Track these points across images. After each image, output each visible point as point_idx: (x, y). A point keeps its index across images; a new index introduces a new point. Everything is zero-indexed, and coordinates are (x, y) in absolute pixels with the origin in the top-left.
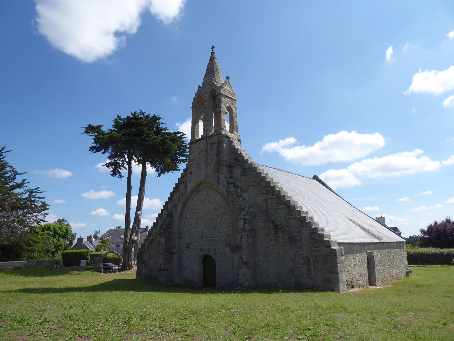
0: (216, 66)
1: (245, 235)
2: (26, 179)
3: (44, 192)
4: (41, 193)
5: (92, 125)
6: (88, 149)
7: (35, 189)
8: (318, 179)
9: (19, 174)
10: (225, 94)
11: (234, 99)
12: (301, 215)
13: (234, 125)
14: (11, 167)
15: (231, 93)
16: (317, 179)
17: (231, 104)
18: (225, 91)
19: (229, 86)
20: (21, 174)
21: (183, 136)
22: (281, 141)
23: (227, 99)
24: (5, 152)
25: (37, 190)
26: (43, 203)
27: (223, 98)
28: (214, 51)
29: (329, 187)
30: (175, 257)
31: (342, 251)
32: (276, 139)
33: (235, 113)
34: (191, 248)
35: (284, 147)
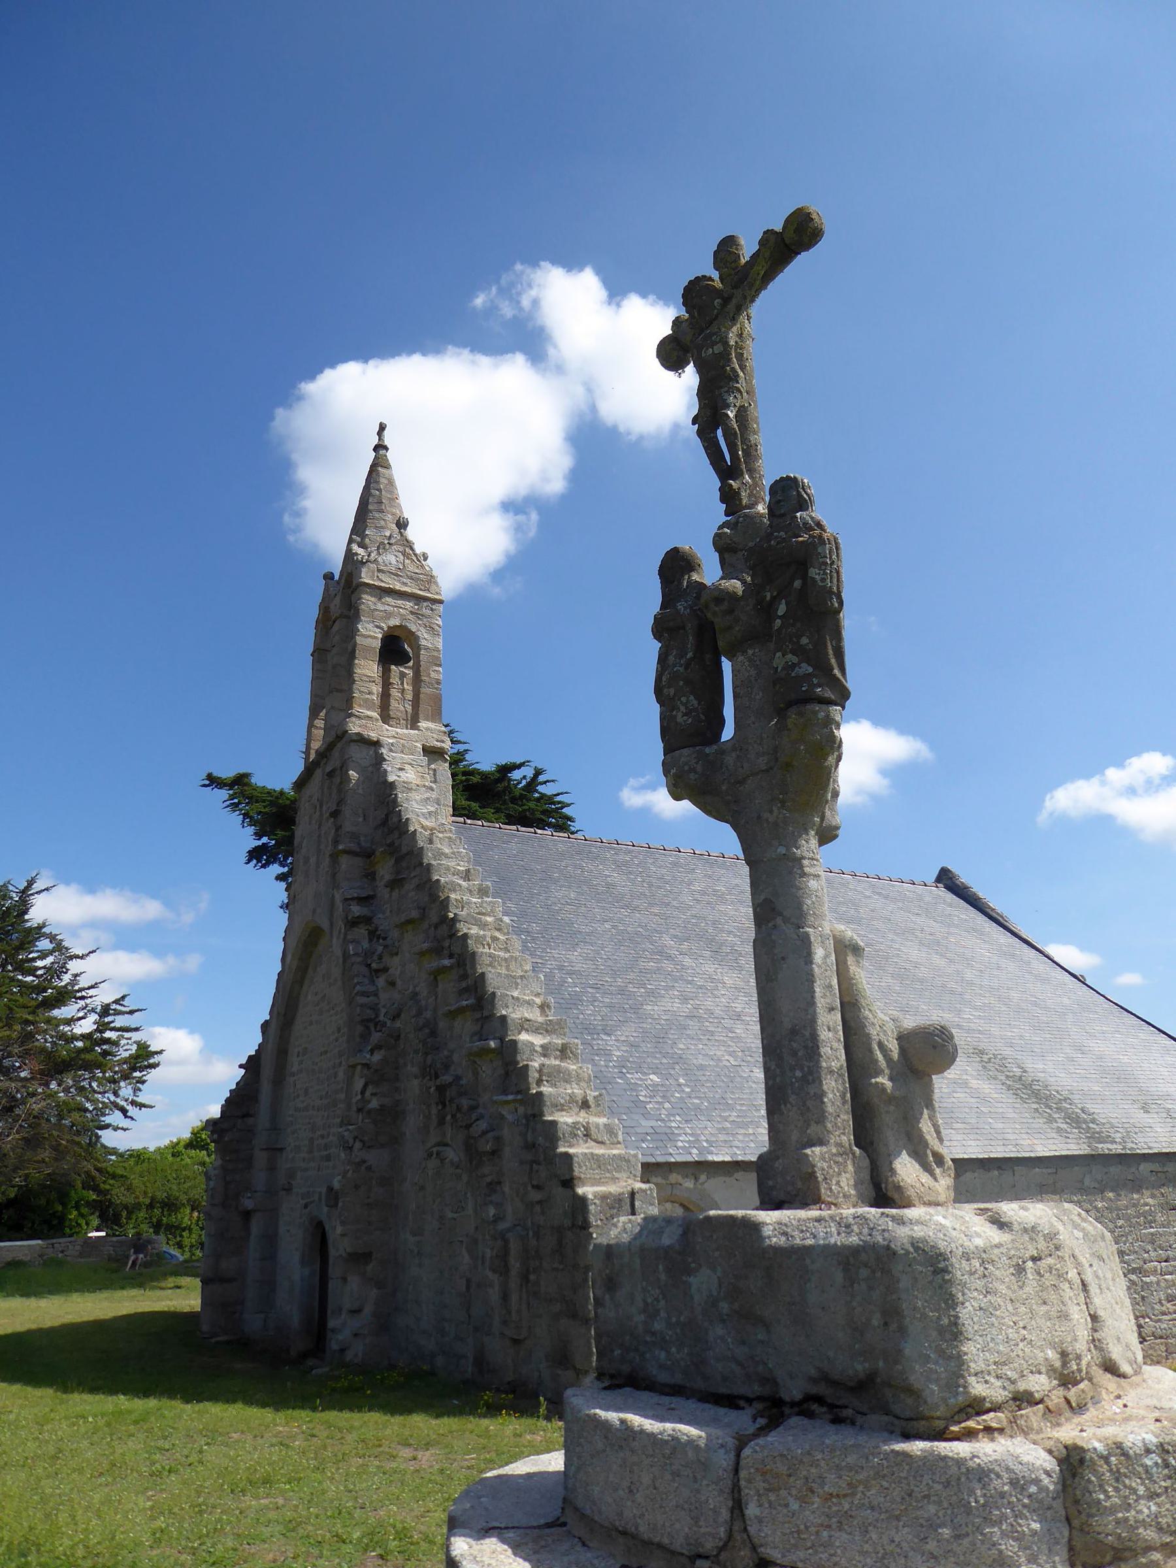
0: (380, 490)
1: (346, 1134)
2: (81, 973)
3: (141, 1010)
4: (131, 1012)
5: (215, 774)
6: (244, 857)
7: (113, 1002)
8: (954, 883)
9: (77, 957)
10: (383, 585)
11: (426, 599)
12: (507, 1035)
13: (421, 696)
14: (52, 938)
15: (411, 578)
16: (949, 882)
17: (411, 617)
18: (379, 571)
19: (404, 554)
20: (82, 957)
21: (541, 778)
22: (1112, 773)
23: (389, 600)
24: (37, 893)
25: (121, 1005)
26: (143, 1048)
27: (369, 598)
28: (387, 442)
29: (998, 914)
30: (256, 1226)
31: (637, 1203)
32: (1091, 768)
33: (427, 649)
34: (295, 1190)
35: (1131, 791)
